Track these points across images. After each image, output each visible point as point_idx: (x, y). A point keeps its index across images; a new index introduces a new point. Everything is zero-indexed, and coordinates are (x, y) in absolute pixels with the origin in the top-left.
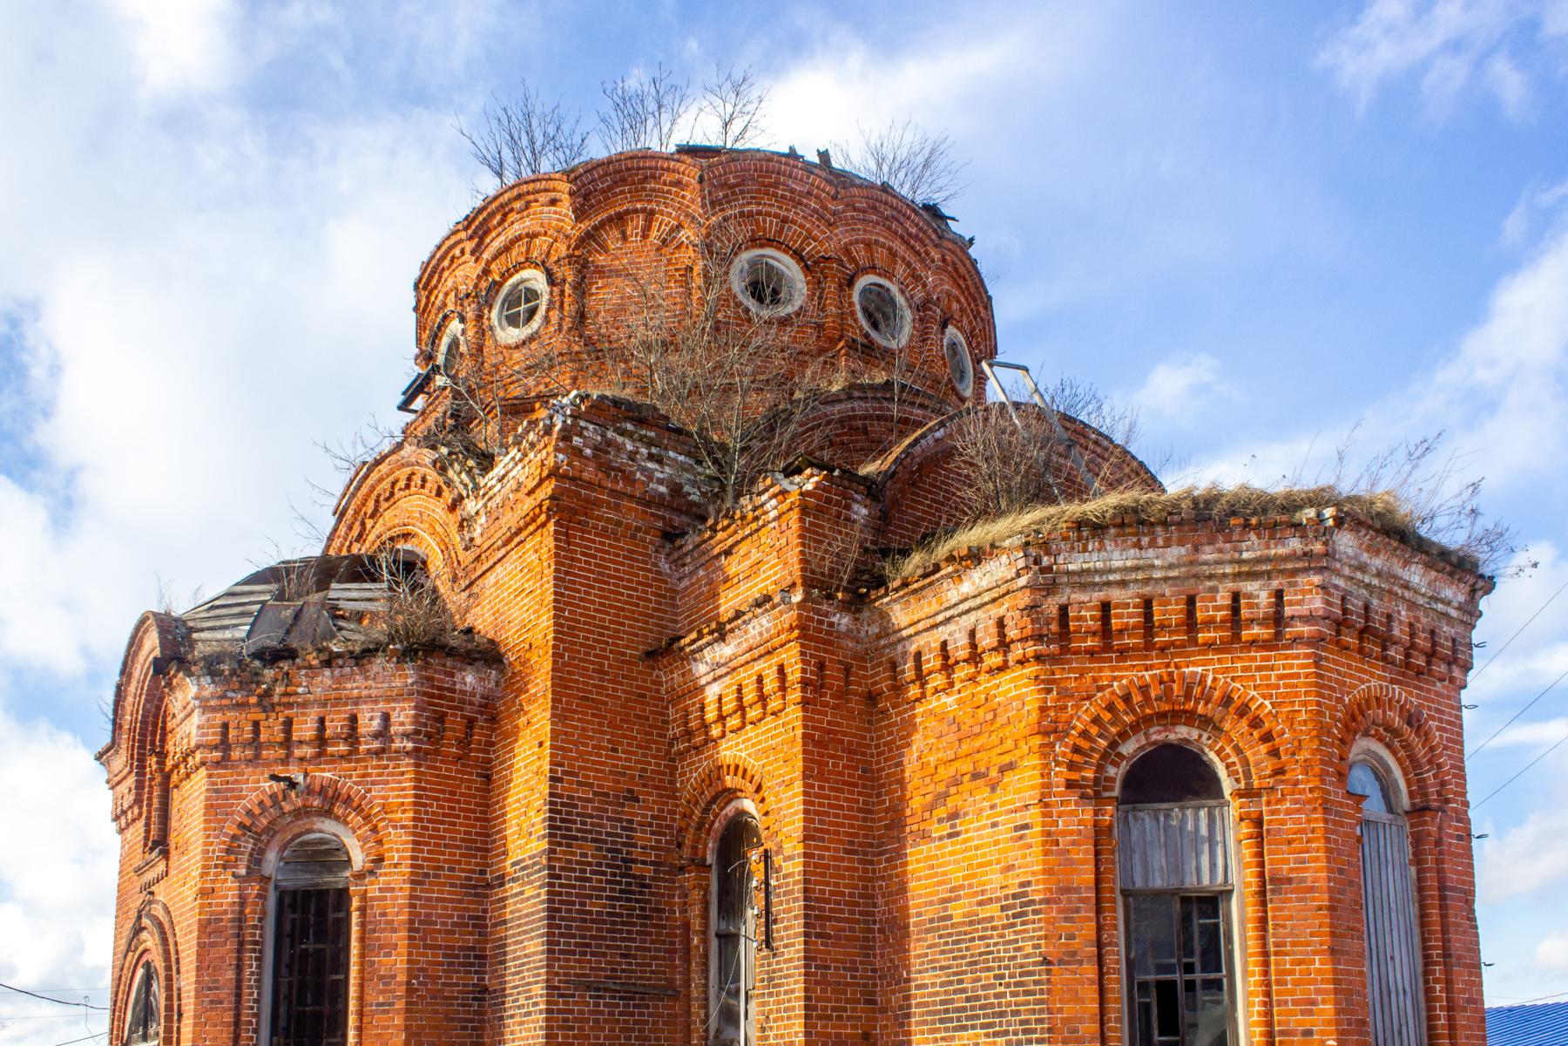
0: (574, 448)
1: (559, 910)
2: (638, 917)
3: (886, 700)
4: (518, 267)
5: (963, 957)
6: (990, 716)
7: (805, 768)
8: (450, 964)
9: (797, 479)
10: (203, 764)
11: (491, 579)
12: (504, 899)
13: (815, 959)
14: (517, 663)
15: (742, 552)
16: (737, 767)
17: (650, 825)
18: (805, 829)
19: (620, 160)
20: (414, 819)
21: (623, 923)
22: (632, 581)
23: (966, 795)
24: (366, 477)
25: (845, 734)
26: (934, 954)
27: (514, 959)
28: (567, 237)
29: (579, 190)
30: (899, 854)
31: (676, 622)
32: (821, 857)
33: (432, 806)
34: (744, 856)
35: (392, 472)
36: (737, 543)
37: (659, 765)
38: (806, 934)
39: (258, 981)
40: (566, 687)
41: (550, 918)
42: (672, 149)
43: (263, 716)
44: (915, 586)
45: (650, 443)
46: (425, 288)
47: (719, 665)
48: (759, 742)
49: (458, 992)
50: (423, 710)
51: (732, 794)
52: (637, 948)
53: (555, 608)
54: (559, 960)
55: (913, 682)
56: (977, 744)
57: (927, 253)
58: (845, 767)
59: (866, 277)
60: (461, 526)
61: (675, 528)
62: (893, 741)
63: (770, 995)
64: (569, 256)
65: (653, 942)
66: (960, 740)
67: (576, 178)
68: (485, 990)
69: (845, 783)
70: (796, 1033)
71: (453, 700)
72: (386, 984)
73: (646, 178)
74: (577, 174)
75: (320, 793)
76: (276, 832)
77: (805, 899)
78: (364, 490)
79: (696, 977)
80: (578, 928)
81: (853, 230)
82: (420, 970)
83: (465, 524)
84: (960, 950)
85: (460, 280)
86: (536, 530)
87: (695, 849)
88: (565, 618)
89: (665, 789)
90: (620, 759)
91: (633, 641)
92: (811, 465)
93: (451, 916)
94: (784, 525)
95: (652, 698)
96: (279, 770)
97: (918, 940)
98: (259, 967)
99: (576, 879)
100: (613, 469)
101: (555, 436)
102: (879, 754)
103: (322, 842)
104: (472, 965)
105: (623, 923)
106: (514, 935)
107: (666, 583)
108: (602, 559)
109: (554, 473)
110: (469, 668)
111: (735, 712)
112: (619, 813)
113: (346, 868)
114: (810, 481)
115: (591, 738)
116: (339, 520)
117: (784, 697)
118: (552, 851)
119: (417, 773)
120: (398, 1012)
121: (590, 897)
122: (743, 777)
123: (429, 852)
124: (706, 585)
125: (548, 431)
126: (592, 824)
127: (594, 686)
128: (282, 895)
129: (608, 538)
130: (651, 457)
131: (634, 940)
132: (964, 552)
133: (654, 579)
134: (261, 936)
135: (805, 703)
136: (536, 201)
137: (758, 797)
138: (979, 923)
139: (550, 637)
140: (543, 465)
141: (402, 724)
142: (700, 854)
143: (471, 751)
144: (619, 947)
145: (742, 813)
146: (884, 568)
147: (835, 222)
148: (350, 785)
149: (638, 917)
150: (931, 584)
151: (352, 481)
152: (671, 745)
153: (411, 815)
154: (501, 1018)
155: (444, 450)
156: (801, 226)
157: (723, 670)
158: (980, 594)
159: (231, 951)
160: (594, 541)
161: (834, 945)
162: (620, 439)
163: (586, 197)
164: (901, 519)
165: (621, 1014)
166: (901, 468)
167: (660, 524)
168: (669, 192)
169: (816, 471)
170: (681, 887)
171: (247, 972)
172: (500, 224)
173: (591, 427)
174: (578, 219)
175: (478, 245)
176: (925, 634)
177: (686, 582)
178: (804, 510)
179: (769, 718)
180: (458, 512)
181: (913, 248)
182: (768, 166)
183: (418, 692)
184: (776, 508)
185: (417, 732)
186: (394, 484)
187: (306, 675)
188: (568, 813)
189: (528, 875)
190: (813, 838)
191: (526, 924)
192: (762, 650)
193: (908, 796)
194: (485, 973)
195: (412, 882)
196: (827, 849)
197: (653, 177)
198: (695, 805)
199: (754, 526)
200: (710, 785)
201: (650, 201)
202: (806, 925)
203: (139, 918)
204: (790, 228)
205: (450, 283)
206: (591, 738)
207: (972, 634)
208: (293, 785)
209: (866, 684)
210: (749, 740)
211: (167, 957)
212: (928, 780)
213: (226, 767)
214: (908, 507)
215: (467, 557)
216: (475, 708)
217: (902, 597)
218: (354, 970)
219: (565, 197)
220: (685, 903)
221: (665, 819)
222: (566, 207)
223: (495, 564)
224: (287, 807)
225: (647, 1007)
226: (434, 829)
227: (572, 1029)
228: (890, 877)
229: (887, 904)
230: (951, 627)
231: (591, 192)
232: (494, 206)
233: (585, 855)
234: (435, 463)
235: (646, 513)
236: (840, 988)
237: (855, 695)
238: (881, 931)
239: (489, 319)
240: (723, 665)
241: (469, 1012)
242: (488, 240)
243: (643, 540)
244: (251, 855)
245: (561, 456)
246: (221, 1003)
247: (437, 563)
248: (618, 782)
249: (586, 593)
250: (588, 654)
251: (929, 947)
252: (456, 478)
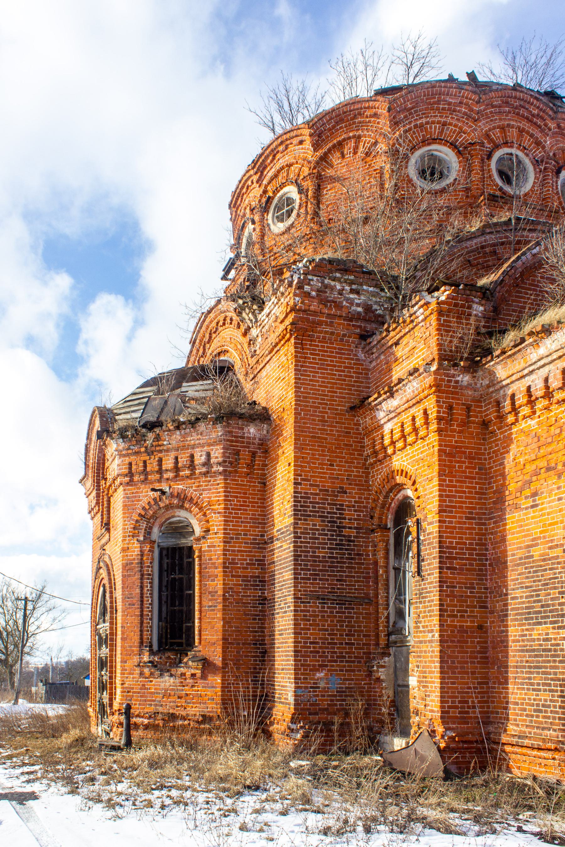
0: (305, 292)
1: (300, 556)
2: (347, 558)
3: (494, 425)
4: (283, 185)
5: (540, 581)
6: (558, 431)
7: (440, 470)
8: (246, 585)
9: (436, 294)
10: (121, 484)
11: (264, 373)
12: (273, 550)
13: (446, 582)
14: (277, 420)
15: (404, 343)
16: (402, 471)
17: (354, 506)
18: (440, 506)
19: (339, 108)
20: (225, 508)
21: (338, 562)
22: (341, 367)
23: (542, 481)
24: (204, 321)
25: (467, 448)
26: (522, 578)
27: (279, 582)
28: (309, 162)
29: (315, 132)
30: (502, 518)
31: (369, 388)
32: (451, 522)
33: (234, 501)
34: (406, 522)
35: (216, 317)
36: (402, 337)
37: (359, 472)
38: (440, 568)
39: (151, 594)
40: (302, 431)
41: (295, 560)
42: (373, 93)
43: (148, 458)
44: (510, 353)
45: (351, 283)
46: (234, 207)
47: (391, 412)
48: (414, 456)
49: (251, 600)
50: (227, 449)
51: (400, 487)
52: (346, 576)
53: (295, 387)
54: (301, 583)
55: (510, 413)
56: (549, 449)
57: (546, 125)
58: (466, 467)
59: (497, 153)
60: (250, 344)
61: (367, 332)
62: (499, 450)
63: (420, 602)
64: (310, 174)
65: (356, 572)
66: (539, 447)
67: (313, 125)
68: (265, 599)
69: (466, 477)
70: (435, 625)
71: (243, 442)
72: (212, 596)
73: (355, 116)
74: (314, 122)
75: (177, 497)
76: (157, 518)
77: (440, 547)
78: (204, 328)
79: (382, 593)
80: (311, 565)
81: (492, 121)
82: (230, 588)
83: (251, 342)
84: (538, 576)
85: (251, 199)
86: (285, 343)
87: (381, 519)
88: (302, 392)
89: (363, 485)
90: (335, 470)
91: (342, 402)
92: (445, 284)
93: (246, 560)
94: (428, 323)
95: (354, 433)
96: (157, 486)
97: (513, 570)
98: (151, 587)
99: (310, 538)
100: (329, 301)
101: (294, 287)
102: (490, 458)
103: (180, 522)
104: (258, 585)
105: (338, 562)
106: (278, 570)
107: (362, 365)
108: (323, 355)
109: (293, 309)
110: (251, 424)
111: (400, 439)
112: (335, 500)
113: (192, 535)
114: (443, 294)
115: (318, 459)
116: (193, 346)
117: (427, 428)
118: (296, 523)
119: (225, 483)
120: (219, 610)
121: (318, 548)
122: (406, 477)
123: (233, 526)
124: (385, 364)
125: (290, 285)
126: (319, 508)
127: (319, 429)
128: (161, 550)
129: (327, 343)
130: (352, 291)
131: (345, 572)
132: (539, 328)
133: (355, 364)
134: (152, 571)
135: (439, 431)
136: (291, 144)
137: (414, 488)
138: (549, 560)
139: (293, 403)
140: (288, 305)
141: (217, 458)
142: (384, 522)
143: (254, 470)
144: (336, 576)
145: (407, 497)
146: (490, 343)
147: (479, 118)
148: (192, 492)
149: (347, 558)
150: (519, 351)
151: (197, 324)
152: (366, 460)
153: (223, 506)
154: (273, 614)
155: (241, 302)
156: (456, 126)
157: (393, 415)
158: (550, 354)
159: (138, 579)
160: (318, 346)
161: (458, 574)
162: (333, 283)
163: (319, 136)
164: (508, 310)
165: (337, 612)
166: (507, 277)
167: (358, 331)
168: (369, 122)
169: (447, 287)
170: (373, 541)
171: (146, 589)
172: (271, 162)
173: (315, 278)
174: (315, 150)
175: (260, 177)
176: (517, 382)
177: (374, 364)
178: (440, 313)
179: (419, 441)
180: (248, 336)
181: (535, 124)
182: (432, 91)
183: (224, 440)
184: (423, 314)
185: (224, 462)
186: (218, 323)
187: (168, 435)
188: (304, 502)
189: (284, 537)
190: (445, 511)
191: (284, 563)
192: (414, 401)
193: (507, 483)
194: (265, 590)
195: (224, 542)
196: (455, 517)
197: (360, 114)
198: (380, 494)
199: (411, 326)
200: (388, 482)
201: (358, 130)
202: (440, 562)
203: (99, 562)
204: (448, 128)
205: (247, 202)
206: (318, 459)
207: (546, 380)
208: (163, 493)
209: (481, 417)
210: (408, 454)
211: (110, 583)
212: (519, 473)
213: (132, 485)
214: (513, 301)
215: (252, 361)
216: (256, 446)
217: (502, 360)
218: (197, 588)
219: (308, 138)
220: (375, 550)
221: (363, 503)
222: (308, 145)
223: (266, 364)
224: (162, 505)
225: (353, 609)
226: (235, 513)
227: (309, 620)
228: (496, 533)
229: (494, 548)
230: (533, 377)
231: (323, 132)
232: (268, 152)
233: (315, 525)
234: (235, 309)
235: (349, 325)
236: (462, 599)
237: (473, 423)
238: (490, 565)
239: (267, 220)
240: (392, 412)
241: (256, 611)
242: (265, 173)
243: (348, 341)
244: (145, 530)
245: (297, 299)
246: (134, 605)
247: (238, 366)
248: (334, 483)
249: (313, 376)
250: (316, 411)
251: (519, 574)
252: (246, 317)
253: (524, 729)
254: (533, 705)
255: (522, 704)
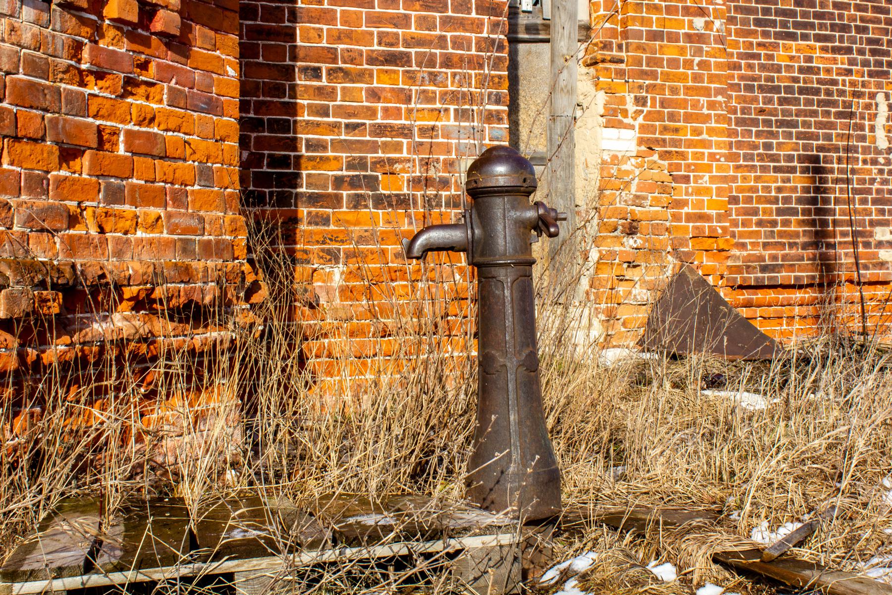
253: (759, 251)
254: (776, 201)
255: (749, 200)
